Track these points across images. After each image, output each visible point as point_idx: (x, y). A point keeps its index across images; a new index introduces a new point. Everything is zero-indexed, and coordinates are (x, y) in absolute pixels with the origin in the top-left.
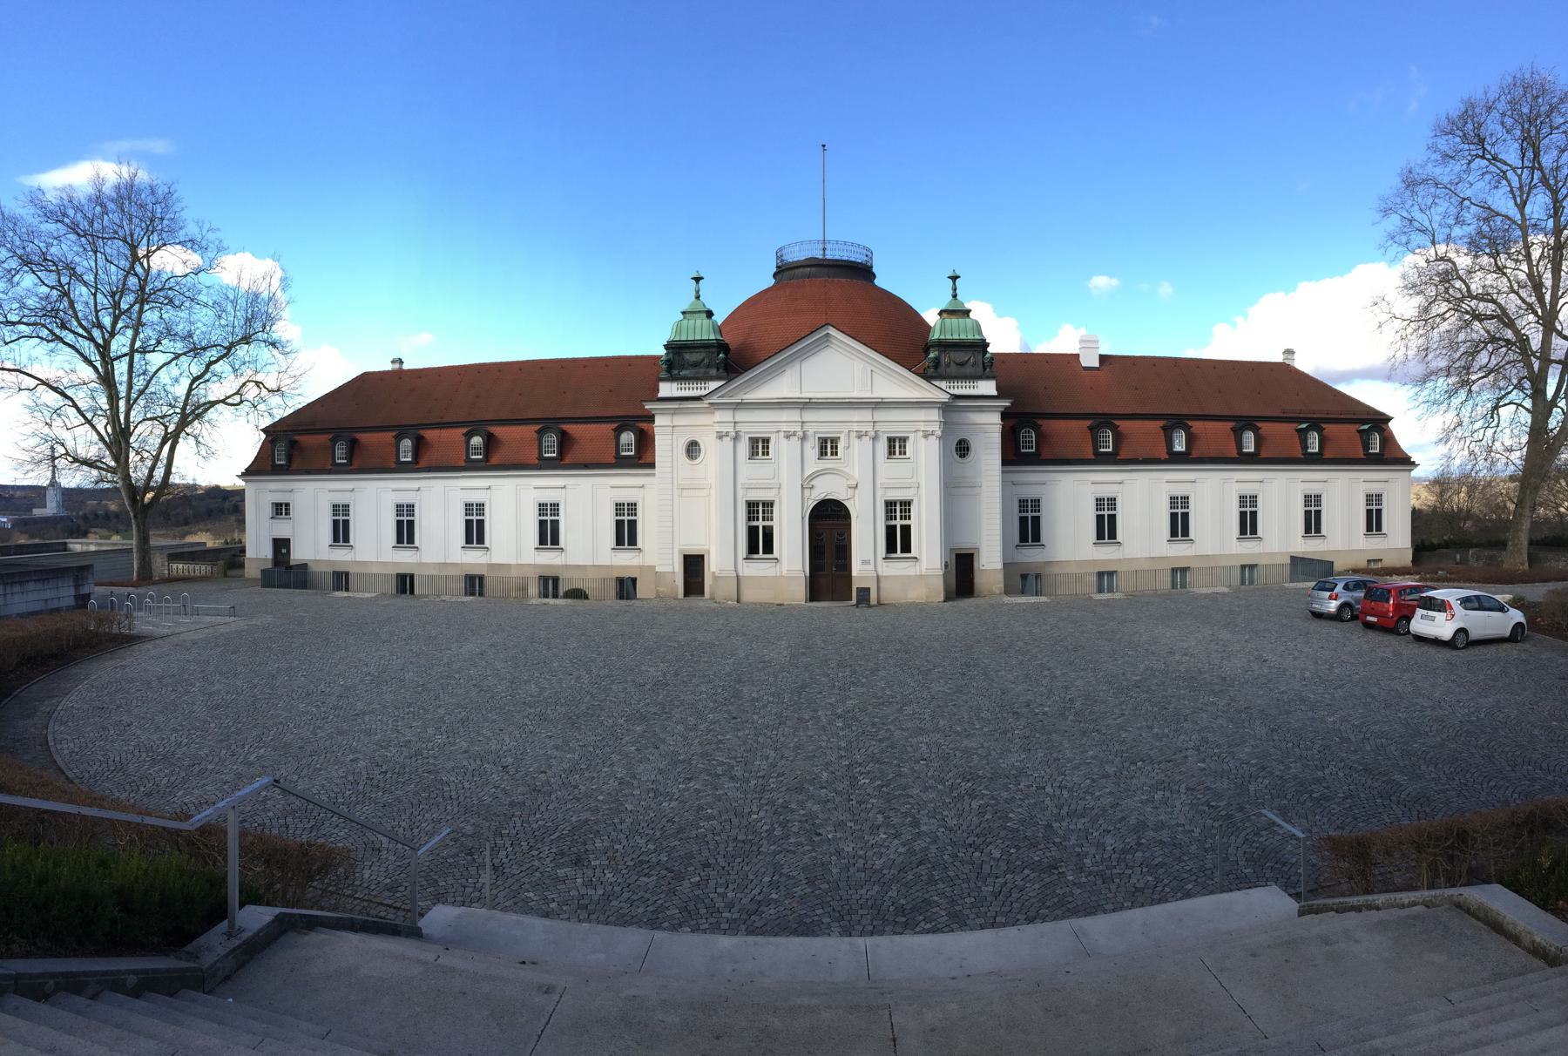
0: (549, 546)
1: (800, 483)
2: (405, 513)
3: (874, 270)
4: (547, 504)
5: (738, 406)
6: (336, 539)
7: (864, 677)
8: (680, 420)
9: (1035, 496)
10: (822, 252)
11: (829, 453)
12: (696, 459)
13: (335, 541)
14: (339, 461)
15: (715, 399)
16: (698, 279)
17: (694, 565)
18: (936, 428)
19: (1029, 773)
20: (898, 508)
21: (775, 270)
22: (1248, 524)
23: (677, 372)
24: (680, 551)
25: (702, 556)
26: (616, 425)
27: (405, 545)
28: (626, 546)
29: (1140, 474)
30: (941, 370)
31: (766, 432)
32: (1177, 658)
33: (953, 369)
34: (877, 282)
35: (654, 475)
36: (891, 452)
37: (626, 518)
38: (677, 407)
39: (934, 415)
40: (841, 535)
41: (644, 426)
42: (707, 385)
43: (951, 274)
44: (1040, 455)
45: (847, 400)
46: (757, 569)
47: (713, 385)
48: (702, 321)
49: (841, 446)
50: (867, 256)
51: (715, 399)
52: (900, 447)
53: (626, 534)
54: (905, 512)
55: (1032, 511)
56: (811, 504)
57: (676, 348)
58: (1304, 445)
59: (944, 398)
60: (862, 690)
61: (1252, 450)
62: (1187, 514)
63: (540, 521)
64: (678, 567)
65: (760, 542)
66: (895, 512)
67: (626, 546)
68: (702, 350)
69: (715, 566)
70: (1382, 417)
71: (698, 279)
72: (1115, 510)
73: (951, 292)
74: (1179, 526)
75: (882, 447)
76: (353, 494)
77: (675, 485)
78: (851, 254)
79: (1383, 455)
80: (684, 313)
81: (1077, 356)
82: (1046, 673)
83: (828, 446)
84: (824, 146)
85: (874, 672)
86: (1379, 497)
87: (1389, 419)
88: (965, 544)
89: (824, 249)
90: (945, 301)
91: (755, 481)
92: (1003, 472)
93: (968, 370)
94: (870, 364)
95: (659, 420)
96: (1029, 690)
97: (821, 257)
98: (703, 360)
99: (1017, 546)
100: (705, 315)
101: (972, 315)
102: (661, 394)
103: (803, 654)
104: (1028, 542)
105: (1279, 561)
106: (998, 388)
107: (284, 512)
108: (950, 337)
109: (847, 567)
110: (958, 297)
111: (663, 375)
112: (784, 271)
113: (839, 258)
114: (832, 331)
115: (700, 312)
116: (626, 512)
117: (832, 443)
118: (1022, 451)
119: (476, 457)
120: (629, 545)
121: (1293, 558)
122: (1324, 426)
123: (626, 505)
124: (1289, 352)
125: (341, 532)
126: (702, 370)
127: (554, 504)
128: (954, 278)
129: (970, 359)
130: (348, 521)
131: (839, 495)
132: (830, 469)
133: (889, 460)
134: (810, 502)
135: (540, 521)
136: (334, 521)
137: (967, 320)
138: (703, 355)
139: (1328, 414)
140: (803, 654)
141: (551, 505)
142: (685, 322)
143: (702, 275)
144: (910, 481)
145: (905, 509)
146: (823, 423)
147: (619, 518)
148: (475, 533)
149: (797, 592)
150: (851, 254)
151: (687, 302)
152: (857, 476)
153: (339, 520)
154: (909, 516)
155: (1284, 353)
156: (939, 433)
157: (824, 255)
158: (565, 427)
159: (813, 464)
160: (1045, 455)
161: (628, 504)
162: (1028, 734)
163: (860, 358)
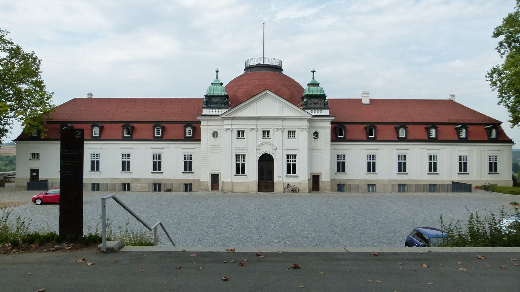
4: (187, 155)
7: (283, 215)
8: (211, 123)
9: (343, 154)
11: (266, 136)
12: (216, 138)
15: (224, 116)
16: (217, 71)
17: (215, 178)
18: (306, 128)
19: (341, 243)
20: (291, 157)
21: (244, 68)
22: (433, 167)
23: (209, 105)
25: (218, 175)
27: (157, 171)
28: (188, 171)
29: (111, 145)
30: (308, 105)
32: (396, 214)
33: (313, 106)
35: (200, 144)
36: (239, 136)
37: (188, 161)
38: (210, 118)
39: (306, 123)
40: (270, 167)
41: (195, 125)
42: (221, 110)
43: (216, 70)
44: (438, 138)
45: (273, 117)
46: (240, 179)
47: (223, 111)
48: (219, 87)
49: (271, 134)
50: (280, 63)
51: (224, 116)
52: (242, 134)
53: (188, 166)
55: (189, 159)
57: (208, 97)
58: (429, 134)
59: (310, 116)
60: (283, 218)
61: (435, 137)
62: (191, 162)
63: (154, 161)
64: (209, 179)
65: (240, 169)
66: (290, 159)
67: (188, 171)
68: (219, 97)
69: (222, 179)
70: (497, 122)
71: (217, 71)
72: (345, 160)
74: (402, 167)
75: (235, 134)
77: (208, 148)
79: (407, 138)
80: (212, 84)
81: (361, 99)
82: (347, 216)
83: (266, 134)
84: (264, 23)
85: (287, 213)
87: (501, 123)
88: (316, 171)
89: (264, 61)
92: (331, 144)
94: (282, 104)
95: (202, 124)
96: (341, 221)
97: (262, 64)
98: (219, 101)
100: (220, 85)
103: (261, 208)
105: (446, 183)
106: (330, 112)
107: (36, 157)
109: (272, 179)
111: (204, 106)
112: (248, 68)
113: (275, 65)
114: (268, 92)
115: (218, 83)
116: (188, 158)
120: (494, 172)
121: (453, 183)
122: (468, 126)
124: (453, 95)
126: (219, 105)
127: (374, 156)
128: (313, 72)
129: (319, 101)
130: (129, 161)
131: (270, 151)
133: (288, 139)
134: (259, 154)
136: (123, 161)
137: (318, 87)
139: (483, 121)
140: (261, 208)
142: (213, 87)
143: (219, 70)
144: (245, 147)
145: (294, 158)
148: (371, 167)
149: (254, 187)
150: (272, 62)
151: (213, 79)
152: (276, 145)
154: (296, 160)
155: (450, 96)
156: (308, 130)
158: (164, 125)
159: (260, 139)
160: (378, 139)
161: (189, 155)
162: (341, 233)
163: (278, 102)
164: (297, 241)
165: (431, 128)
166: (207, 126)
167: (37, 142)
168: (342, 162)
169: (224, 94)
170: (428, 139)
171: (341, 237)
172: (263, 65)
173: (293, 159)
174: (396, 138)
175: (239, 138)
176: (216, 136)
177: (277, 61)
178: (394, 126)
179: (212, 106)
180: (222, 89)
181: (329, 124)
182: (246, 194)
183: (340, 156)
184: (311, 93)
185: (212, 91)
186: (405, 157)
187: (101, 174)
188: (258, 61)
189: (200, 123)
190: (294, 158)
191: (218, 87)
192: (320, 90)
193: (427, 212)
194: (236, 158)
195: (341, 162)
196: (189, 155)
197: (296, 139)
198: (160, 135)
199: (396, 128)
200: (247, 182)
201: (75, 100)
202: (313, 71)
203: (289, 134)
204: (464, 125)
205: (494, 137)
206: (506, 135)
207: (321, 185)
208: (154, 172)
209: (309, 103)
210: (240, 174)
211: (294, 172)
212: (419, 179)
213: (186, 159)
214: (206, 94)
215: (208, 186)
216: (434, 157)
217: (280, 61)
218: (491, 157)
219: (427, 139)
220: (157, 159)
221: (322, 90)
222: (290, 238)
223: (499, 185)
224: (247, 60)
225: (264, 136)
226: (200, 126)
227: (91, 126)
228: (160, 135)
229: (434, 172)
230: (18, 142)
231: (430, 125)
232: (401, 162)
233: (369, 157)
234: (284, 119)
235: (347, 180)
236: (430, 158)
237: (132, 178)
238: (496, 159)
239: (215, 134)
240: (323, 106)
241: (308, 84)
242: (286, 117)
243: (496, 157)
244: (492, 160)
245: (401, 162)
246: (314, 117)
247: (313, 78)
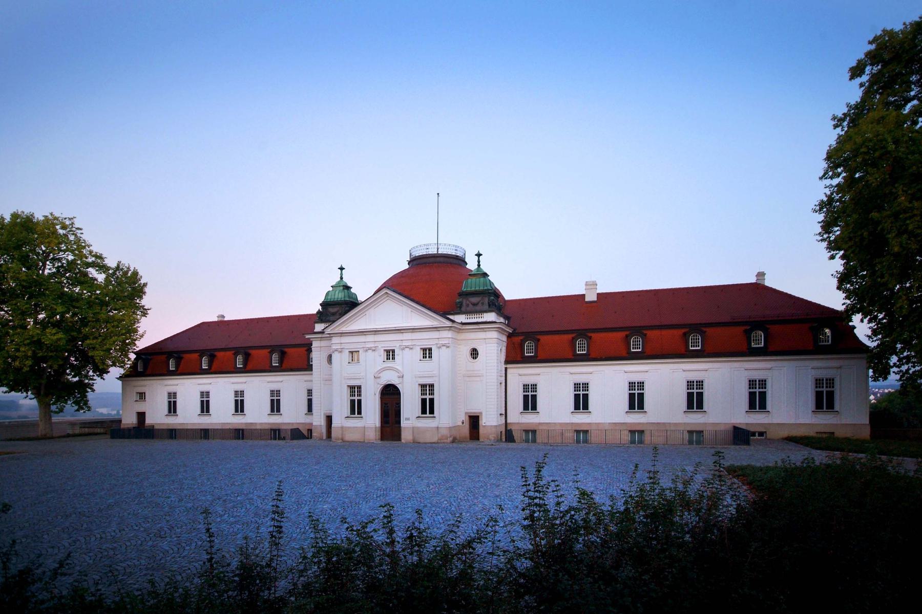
0: (205, 413)
2: (275, 395)
6: (272, 410)
9: (174, 391)
12: (476, 358)
13: (272, 412)
14: (275, 365)
24: (324, 415)
27: (172, 414)
29: (189, 380)
31: (357, 348)
35: (312, 374)
46: (355, 423)
54: (424, 391)
55: (531, 392)
56: (380, 387)
62: (209, 401)
63: (630, 393)
65: (356, 408)
66: (426, 391)
68: (337, 306)
76: (177, 386)
83: (390, 354)
84: (438, 194)
86: (242, 392)
91: (353, 375)
99: (521, 413)
102: (316, 330)
104: (529, 410)
108: (470, 289)
110: (481, 266)
117: (429, 351)
124: (841, 265)
125: (172, 408)
128: (342, 269)
131: (395, 381)
132: (389, 367)
135: (630, 393)
136: (235, 400)
138: (338, 308)
141: (583, 384)
145: (424, 391)
146: (390, 341)
147: (576, 393)
148: (581, 402)
163: (366, 310)
167: (144, 378)
168: (638, 393)
173: (429, 391)
176: (476, 355)
182: (361, 446)
183: (580, 384)
184: (469, 289)
186: (642, 385)
187: (178, 418)
195: (530, 396)
198: (640, 349)
201: (203, 323)
204: (759, 325)
205: (761, 346)
206: (858, 338)
207: (482, 431)
208: (687, 412)
209: (464, 304)
211: (432, 412)
213: (585, 391)
215: (323, 433)
216: (584, 386)
218: (633, 385)
223: (840, 433)
230: (122, 379)
233: (577, 386)
234: (414, 330)
243: (763, 383)
244: (529, 392)
245: (204, 401)
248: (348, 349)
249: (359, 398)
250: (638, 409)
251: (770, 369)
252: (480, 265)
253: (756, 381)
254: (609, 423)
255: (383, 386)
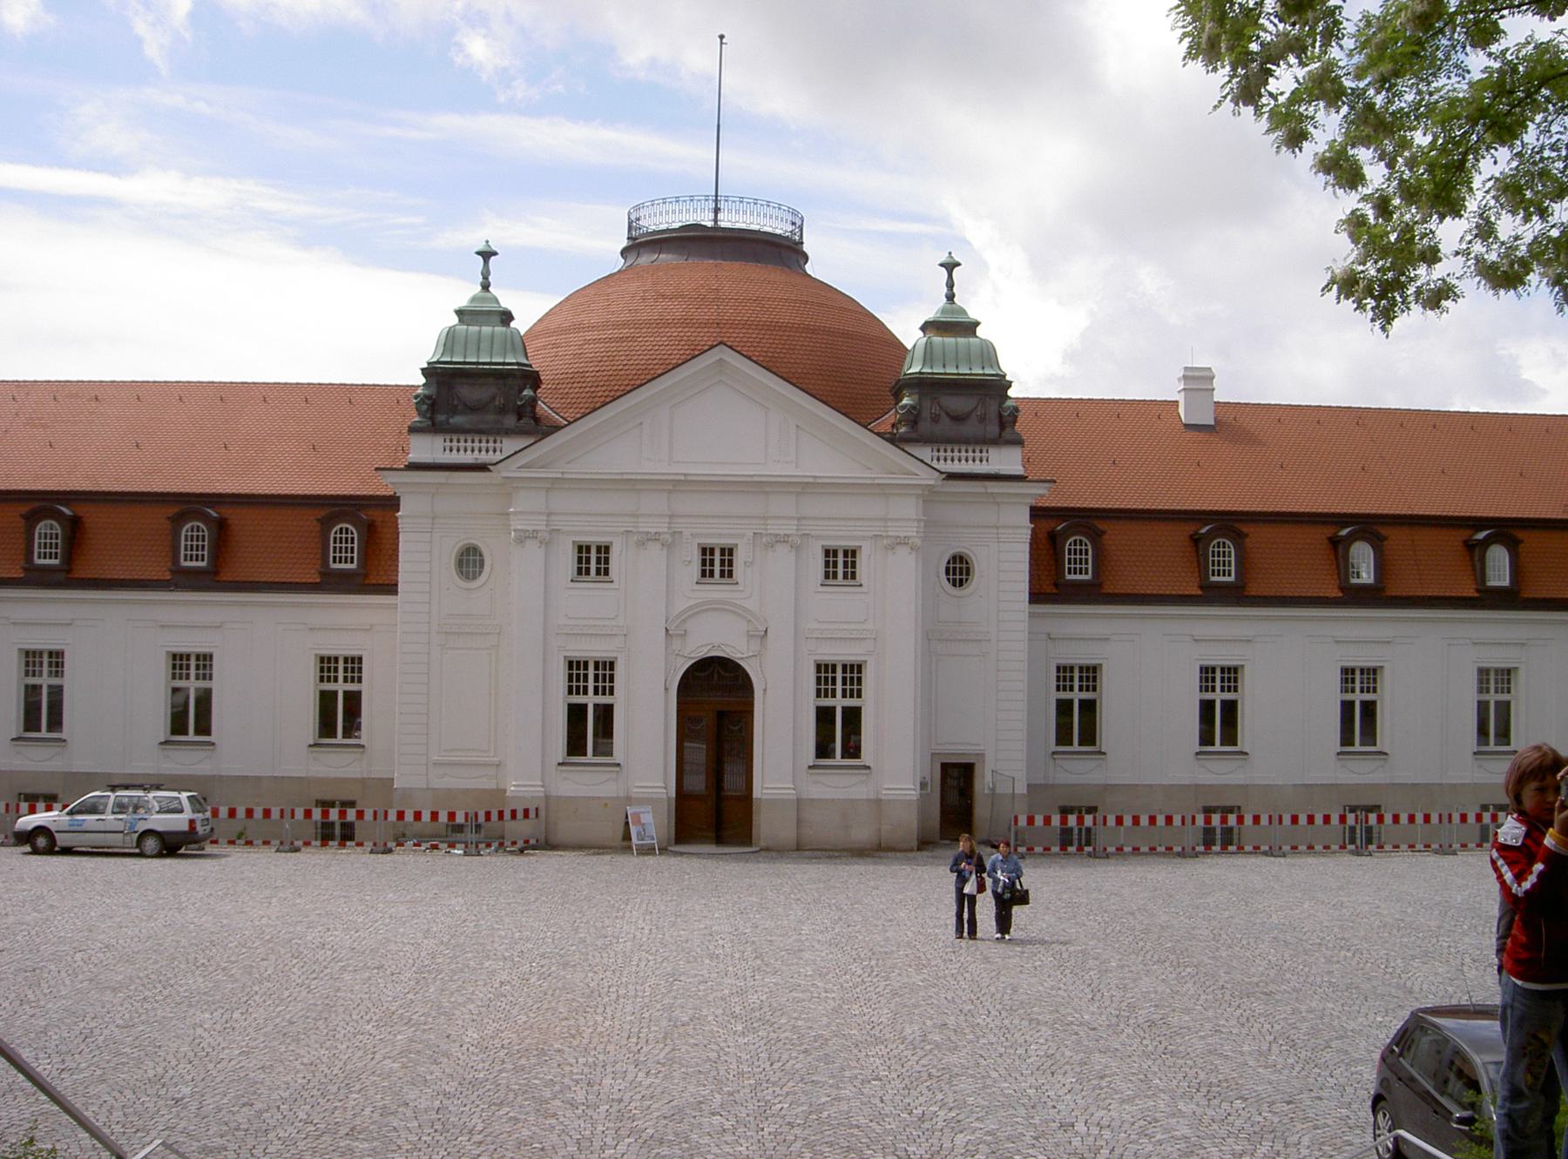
1: (663, 625)
3: (806, 248)
4: (336, 659)
5: (554, 485)
10: (712, 216)
12: (474, 578)
13: (174, 731)
14: (42, 561)
18: (911, 531)
21: (624, 243)
26: (176, 510)
30: (925, 426)
34: (809, 268)
42: (984, 454)
47: (509, 445)
59: (927, 478)
63: (27, 686)
68: (491, 380)
69: (983, 783)
73: (945, 290)
78: (768, 221)
79: (1100, 585)
84: (722, 37)
88: (959, 745)
89: (717, 210)
90: (932, 309)
92: (1032, 615)
93: (970, 428)
97: (710, 224)
98: (494, 398)
100: (497, 319)
101: (980, 331)
104: (1071, 744)
110: (955, 299)
112: (640, 244)
113: (743, 226)
115: (489, 313)
118: (1069, 577)
119: (47, 561)
120: (198, 732)
123: (839, 670)
126: (491, 417)
128: (950, 266)
129: (975, 408)
131: (735, 647)
133: (699, 587)
137: (972, 340)
147: (32, 681)
150: (664, 218)
151: (464, 293)
153: (1071, 702)
156: (918, 542)
157: (716, 220)
160: (1254, 589)
164: (824, 1099)
165: (1355, 540)
166: (995, 531)
169: (518, 364)
170: (1476, 595)
171: (1053, 1074)
172: (716, 228)
173: (844, 683)
174: (1336, 590)
175: (584, 578)
177: (780, 214)
178: (1187, 528)
179: (457, 420)
180: (509, 336)
181: (1023, 518)
185: (459, 348)
188: (695, 211)
189: (399, 505)
190: (578, 675)
191: (486, 330)
192: (982, 348)
193: (1467, 940)
194: (570, 676)
196: (1081, 669)
197: (859, 589)
198: (1086, 573)
199: (1196, 540)
200: (621, 794)
202: (949, 260)
203: (827, 564)
207: (981, 810)
209: (926, 414)
210: (585, 754)
211: (852, 750)
212: (1439, 782)
214: (429, 363)
217: (795, 213)
219: (1471, 593)
220: (341, 679)
221: (988, 354)
222: (791, 1084)
224: (637, 208)
225: (706, 573)
226: (397, 518)
227: (22, 516)
228: (1086, 573)
229: (1362, 744)
231: (1351, 524)
232: (1352, 703)
235: (1108, 788)
236: (329, 671)
237: (66, 770)
238: (31, 659)
239: (468, 561)
240: (993, 429)
241: (926, 323)
242: (815, 477)
246: (951, 482)
247: (950, 297)
248: (819, 537)
249: (851, 702)
250: (1080, 744)
251: (219, 627)
252: (954, 296)
253: (834, 667)
254: (1295, 785)
255: (693, 661)
